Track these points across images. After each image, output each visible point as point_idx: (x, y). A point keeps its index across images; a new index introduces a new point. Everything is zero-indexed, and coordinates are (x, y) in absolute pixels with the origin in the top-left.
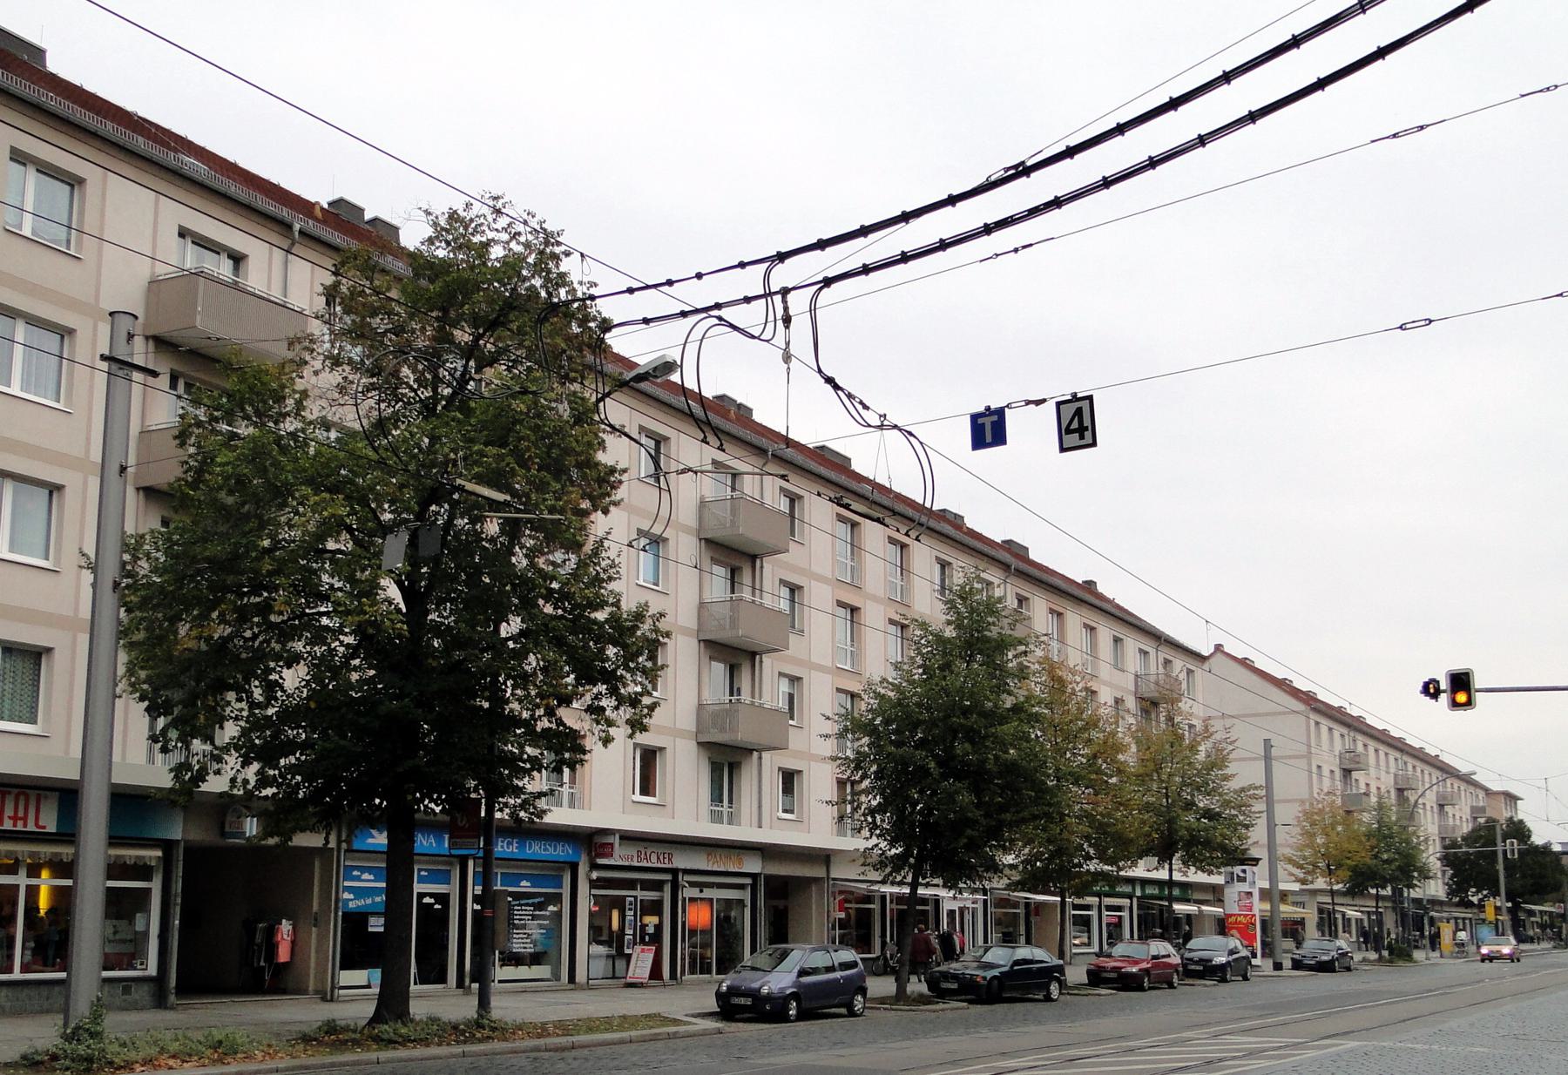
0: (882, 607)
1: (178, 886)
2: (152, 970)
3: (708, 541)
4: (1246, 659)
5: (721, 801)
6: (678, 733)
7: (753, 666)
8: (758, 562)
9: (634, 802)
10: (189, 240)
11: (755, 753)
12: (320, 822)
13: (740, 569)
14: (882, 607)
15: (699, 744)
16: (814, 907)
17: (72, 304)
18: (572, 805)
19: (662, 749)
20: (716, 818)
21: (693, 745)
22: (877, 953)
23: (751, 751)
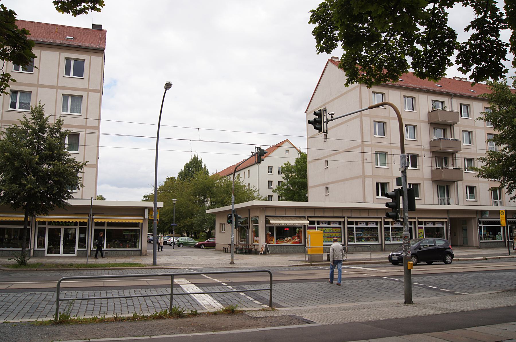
0: (484, 130)
1: (449, 228)
2: (502, 240)
3: (431, 123)
4: (455, 77)
5: (444, 196)
6: (423, 179)
7: (453, 157)
8: (452, 126)
9: (467, 201)
10: (406, 98)
11: (455, 182)
12: (32, 214)
13: (446, 129)
14: (484, 130)
15: (433, 181)
16: (473, 224)
17: (384, 117)
18: (501, 205)
19: (420, 184)
20: (440, 202)
21: (431, 182)
22: (379, 242)
23: (454, 182)
